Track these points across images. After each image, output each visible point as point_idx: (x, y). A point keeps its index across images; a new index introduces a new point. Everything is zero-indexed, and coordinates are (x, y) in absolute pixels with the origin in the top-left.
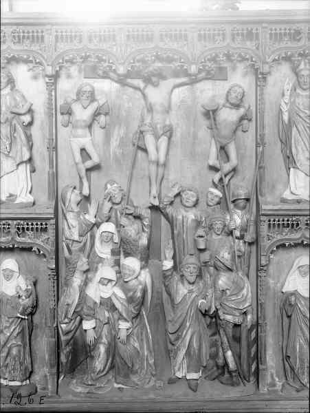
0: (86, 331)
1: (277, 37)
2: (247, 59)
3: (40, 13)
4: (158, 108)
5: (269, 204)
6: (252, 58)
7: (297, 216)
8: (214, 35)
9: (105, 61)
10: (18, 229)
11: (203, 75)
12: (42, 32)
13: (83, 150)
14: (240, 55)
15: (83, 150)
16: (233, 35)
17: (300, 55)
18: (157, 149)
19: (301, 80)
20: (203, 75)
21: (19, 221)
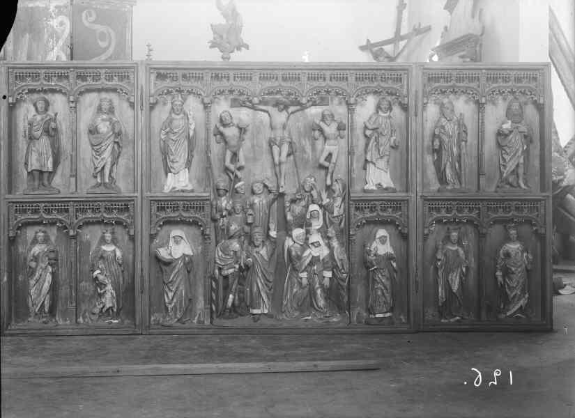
0: (324, 277)
1: (311, 78)
2: (340, 94)
3: (178, 63)
4: (278, 126)
5: (356, 192)
6: (296, 93)
7: (175, 201)
8: (52, 76)
9: (292, 95)
10: (106, 208)
11: (311, 103)
12: (299, 74)
13: (330, 155)
14: (239, 91)
15: (330, 155)
16: (331, 78)
17: (177, 91)
18: (280, 155)
19: (175, 108)
20: (311, 103)
21: (46, 204)
